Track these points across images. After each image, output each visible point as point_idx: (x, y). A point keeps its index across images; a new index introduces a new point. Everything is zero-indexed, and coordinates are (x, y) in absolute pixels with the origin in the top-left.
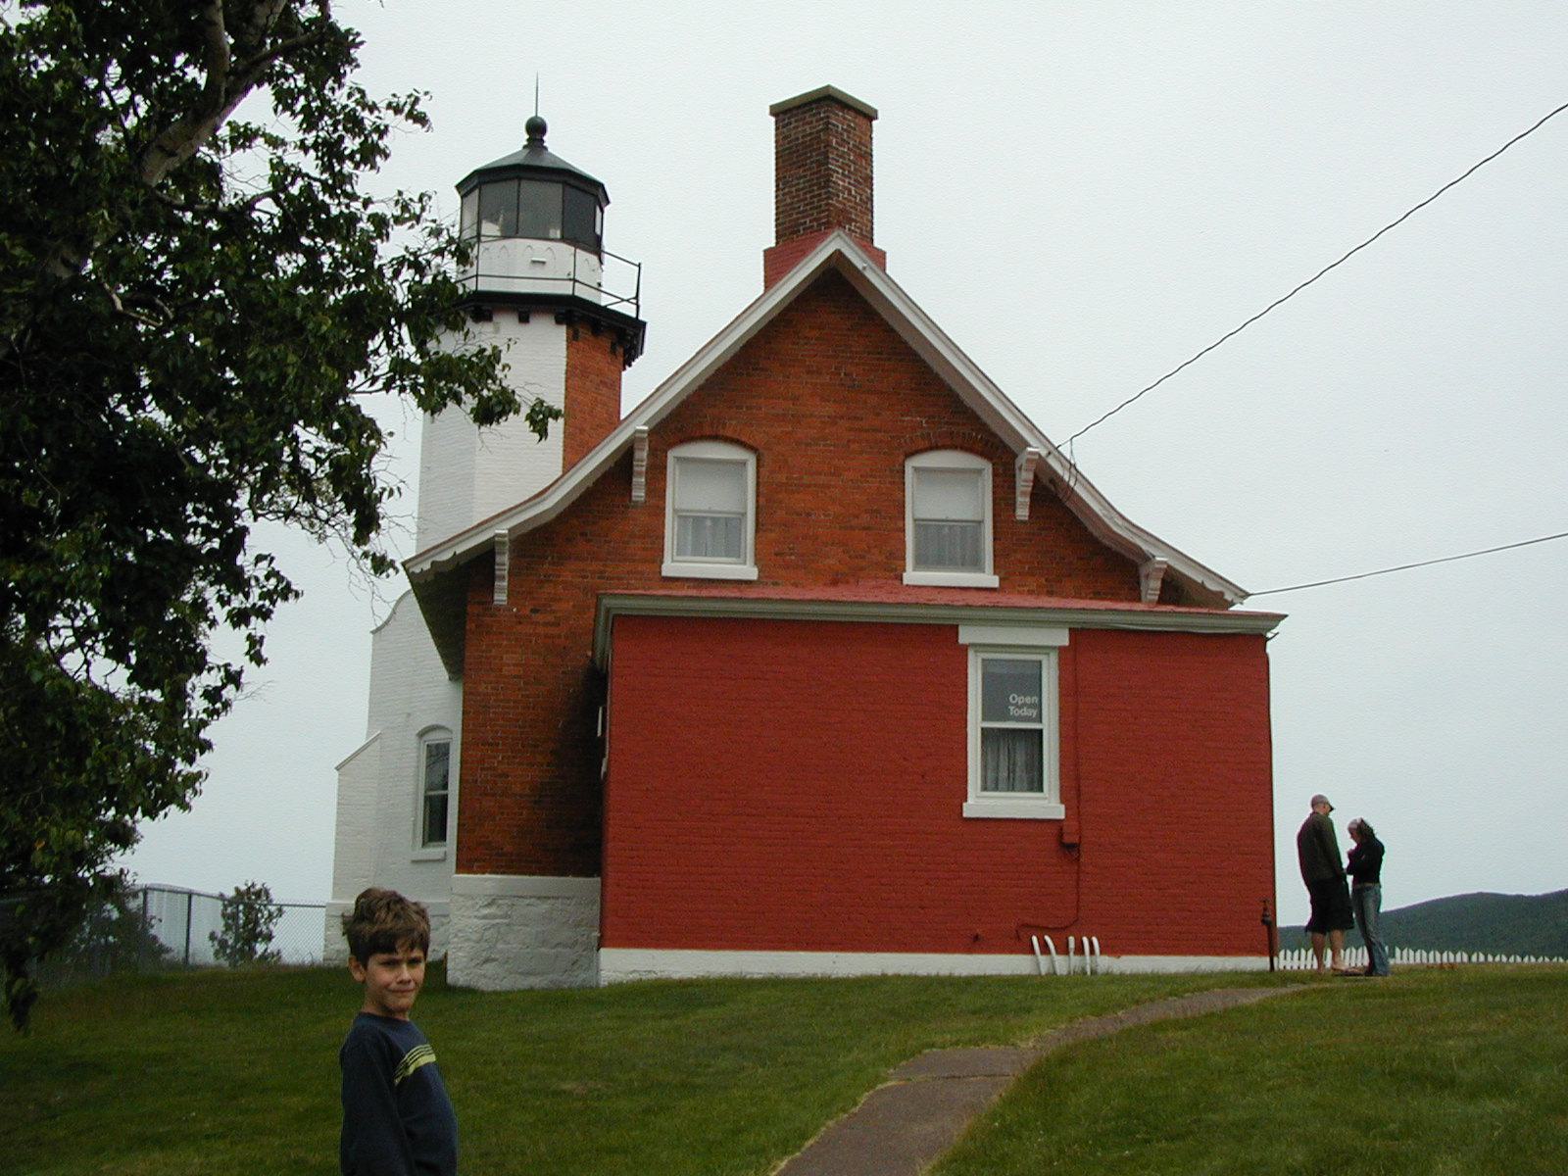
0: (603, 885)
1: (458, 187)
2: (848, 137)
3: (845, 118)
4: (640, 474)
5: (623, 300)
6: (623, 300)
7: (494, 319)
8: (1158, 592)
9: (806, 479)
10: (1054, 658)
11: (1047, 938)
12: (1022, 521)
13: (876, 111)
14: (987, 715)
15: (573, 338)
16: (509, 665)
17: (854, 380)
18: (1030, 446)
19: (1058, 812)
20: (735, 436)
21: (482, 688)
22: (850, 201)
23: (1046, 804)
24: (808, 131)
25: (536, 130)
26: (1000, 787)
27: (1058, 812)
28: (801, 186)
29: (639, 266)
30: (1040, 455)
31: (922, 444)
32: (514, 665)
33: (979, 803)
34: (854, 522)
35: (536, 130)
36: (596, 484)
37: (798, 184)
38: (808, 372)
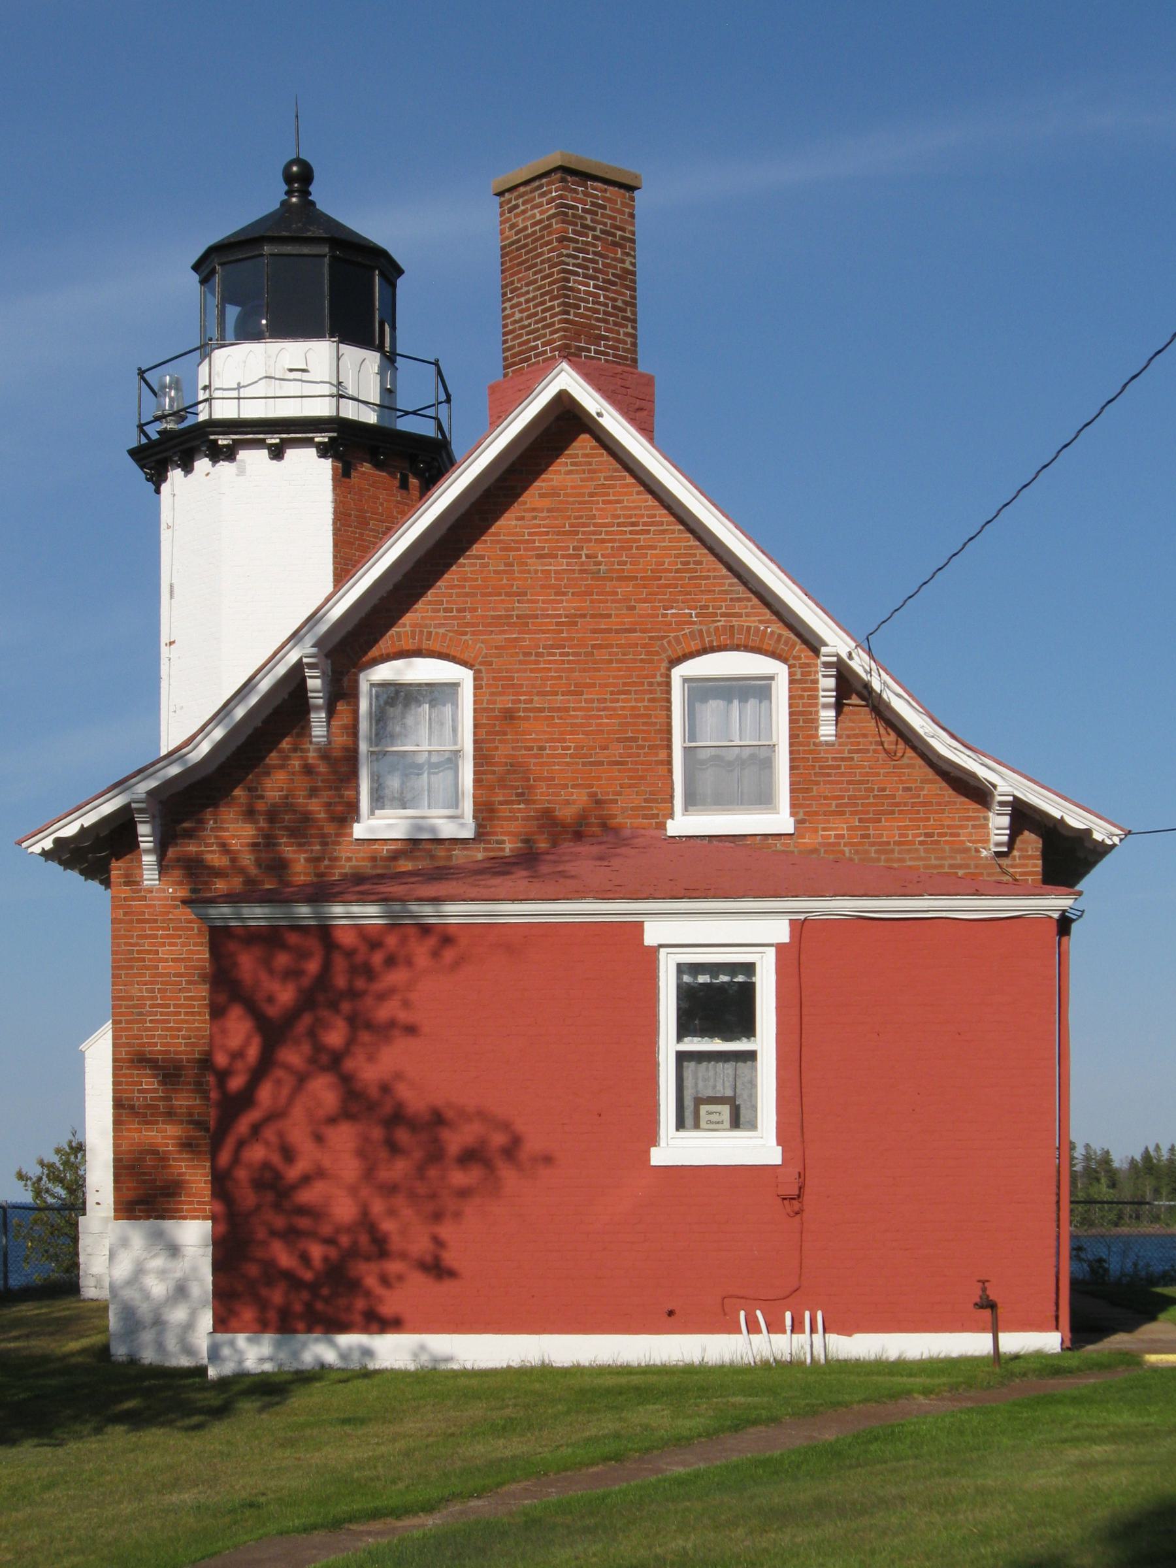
0: (6, 1278)
1: (196, 267)
2: (592, 221)
3: (586, 194)
4: (318, 708)
5: (414, 413)
6: (414, 413)
7: (238, 457)
8: (1008, 832)
9: (538, 702)
10: (771, 953)
11: (758, 1313)
12: (827, 743)
13: (636, 177)
14: (683, 1031)
15: (342, 477)
16: (166, 960)
17: (599, 564)
18: (826, 645)
19: (772, 1155)
20: (445, 651)
21: (135, 991)
22: (597, 311)
23: (759, 1146)
24: (538, 217)
25: (300, 177)
26: (703, 1124)
27: (772, 1155)
28: (531, 295)
29: (436, 364)
30: (837, 655)
31: (694, 645)
32: (174, 960)
33: (675, 1148)
34: (602, 756)
35: (300, 177)
36: (266, 722)
37: (528, 292)
38: (539, 557)
